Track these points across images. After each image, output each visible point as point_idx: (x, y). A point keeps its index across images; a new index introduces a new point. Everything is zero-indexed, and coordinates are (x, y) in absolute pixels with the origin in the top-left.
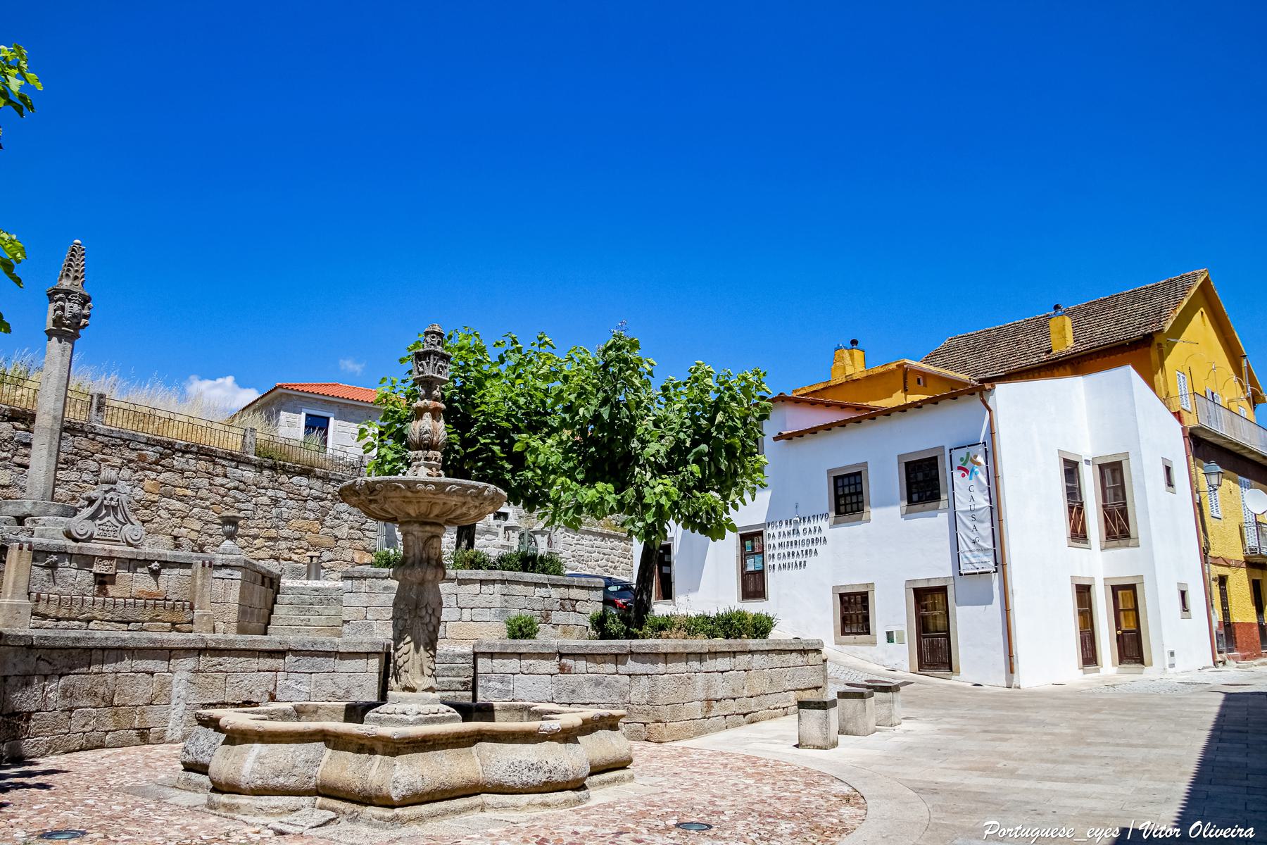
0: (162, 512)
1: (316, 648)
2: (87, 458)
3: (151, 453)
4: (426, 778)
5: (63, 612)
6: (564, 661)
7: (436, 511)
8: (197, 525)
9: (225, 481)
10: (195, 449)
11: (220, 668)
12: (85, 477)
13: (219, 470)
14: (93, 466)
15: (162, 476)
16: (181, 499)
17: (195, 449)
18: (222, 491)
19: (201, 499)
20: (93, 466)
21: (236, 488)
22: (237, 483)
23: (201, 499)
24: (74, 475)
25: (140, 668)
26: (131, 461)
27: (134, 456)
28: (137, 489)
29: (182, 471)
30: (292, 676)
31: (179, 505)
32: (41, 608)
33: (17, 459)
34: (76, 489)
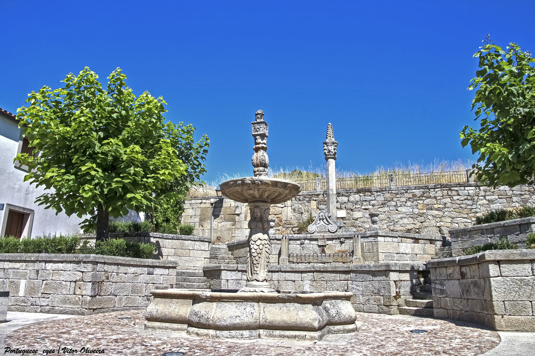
0: (429, 217)
1: (362, 269)
2: (390, 201)
3: (418, 192)
4: (159, 312)
5: (299, 260)
6: (463, 269)
7: (266, 194)
8: (449, 220)
9: (459, 197)
10: (439, 186)
11: (323, 279)
12: (391, 208)
13: (454, 193)
14: (394, 203)
15: (425, 202)
16: (438, 209)
17: (439, 186)
18: (458, 202)
19: (448, 208)
20: (394, 203)
21: (465, 199)
22: (466, 197)
23: (448, 208)
24: (386, 209)
25: (290, 278)
26: (409, 198)
27: (411, 196)
28: (415, 209)
29: (435, 197)
30: (354, 283)
31: (436, 212)
32: (291, 259)
33: (363, 207)
34: (389, 214)
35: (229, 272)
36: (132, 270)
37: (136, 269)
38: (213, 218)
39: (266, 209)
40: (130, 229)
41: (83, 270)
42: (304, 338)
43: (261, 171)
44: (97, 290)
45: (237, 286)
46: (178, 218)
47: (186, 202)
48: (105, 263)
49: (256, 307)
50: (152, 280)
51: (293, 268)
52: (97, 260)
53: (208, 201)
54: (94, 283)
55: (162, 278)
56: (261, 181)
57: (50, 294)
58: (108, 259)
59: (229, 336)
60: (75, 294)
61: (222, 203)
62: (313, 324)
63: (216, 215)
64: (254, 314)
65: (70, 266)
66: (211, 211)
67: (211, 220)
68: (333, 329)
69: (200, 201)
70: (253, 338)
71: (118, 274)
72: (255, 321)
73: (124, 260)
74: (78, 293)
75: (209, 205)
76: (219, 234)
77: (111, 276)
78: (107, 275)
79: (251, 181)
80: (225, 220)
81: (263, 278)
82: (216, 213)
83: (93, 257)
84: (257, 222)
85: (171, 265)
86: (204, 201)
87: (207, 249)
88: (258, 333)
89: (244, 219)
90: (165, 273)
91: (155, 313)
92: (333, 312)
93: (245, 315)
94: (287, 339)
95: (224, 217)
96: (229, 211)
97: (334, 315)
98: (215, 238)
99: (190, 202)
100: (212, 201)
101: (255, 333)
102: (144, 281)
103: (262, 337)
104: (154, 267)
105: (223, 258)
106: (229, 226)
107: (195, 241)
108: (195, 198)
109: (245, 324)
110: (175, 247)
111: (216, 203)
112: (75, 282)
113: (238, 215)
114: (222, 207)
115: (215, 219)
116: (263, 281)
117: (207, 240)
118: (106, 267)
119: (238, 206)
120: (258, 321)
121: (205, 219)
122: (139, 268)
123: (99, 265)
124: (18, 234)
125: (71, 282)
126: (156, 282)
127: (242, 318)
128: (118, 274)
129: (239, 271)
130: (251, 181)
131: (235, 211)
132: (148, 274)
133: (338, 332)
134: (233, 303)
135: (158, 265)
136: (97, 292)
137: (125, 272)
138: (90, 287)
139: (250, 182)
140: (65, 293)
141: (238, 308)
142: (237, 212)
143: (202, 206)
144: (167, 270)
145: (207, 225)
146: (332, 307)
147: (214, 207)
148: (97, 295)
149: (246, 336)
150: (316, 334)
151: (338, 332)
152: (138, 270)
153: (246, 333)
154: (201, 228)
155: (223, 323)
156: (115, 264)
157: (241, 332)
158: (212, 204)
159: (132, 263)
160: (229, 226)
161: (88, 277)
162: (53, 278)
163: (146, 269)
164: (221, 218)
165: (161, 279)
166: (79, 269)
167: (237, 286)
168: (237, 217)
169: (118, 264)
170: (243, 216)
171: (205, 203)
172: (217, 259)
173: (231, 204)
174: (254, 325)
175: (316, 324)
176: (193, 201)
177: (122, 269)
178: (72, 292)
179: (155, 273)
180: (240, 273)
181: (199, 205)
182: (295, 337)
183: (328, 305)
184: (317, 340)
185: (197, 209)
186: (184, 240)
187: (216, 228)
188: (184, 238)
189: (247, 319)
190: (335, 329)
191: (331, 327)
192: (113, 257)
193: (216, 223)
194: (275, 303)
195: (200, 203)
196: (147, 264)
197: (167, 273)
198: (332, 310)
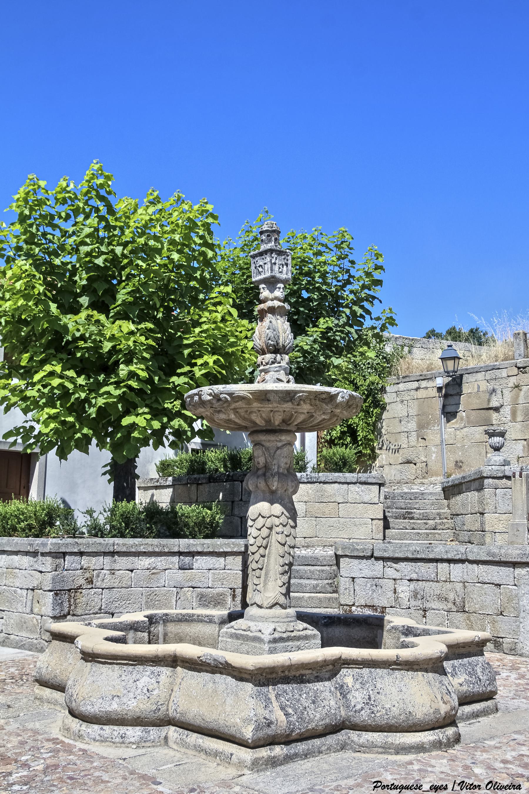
35: (356, 561)
36: (146, 562)
37: (153, 559)
38: (444, 420)
39: (278, 448)
40: (225, 467)
41: (40, 569)
42: (228, 759)
43: (267, 364)
44: (66, 604)
45: (374, 591)
46: (374, 425)
47: (388, 389)
48: (81, 554)
49: (163, 679)
50: (189, 580)
51: (494, 555)
52: (63, 550)
53: (430, 384)
54: (57, 593)
55: (210, 576)
56: (231, 394)
57: (4, 611)
58: (88, 545)
59: (98, 738)
60: (32, 612)
61: (460, 385)
62: (244, 730)
63: (449, 414)
64: (155, 692)
65: (26, 561)
66: (438, 403)
67: (440, 424)
68: (356, 739)
69: (415, 385)
70: (148, 744)
71: (112, 571)
72: (154, 707)
73: (124, 545)
74: (36, 610)
75: (434, 393)
76: (459, 455)
77: (98, 576)
78: (88, 575)
79: (210, 395)
80: (469, 422)
81: (272, 601)
82: (449, 409)
83: (51, 544)
84: (258, 477)
85: (229, 550)
86: (424, 384)
87: (376, 500)
88: (163, 735)
89: (509, 417)
90: (217, 566)
91: (44, 671)
92: (357, 698)
93: (131, 695)
94: (204, 757)
95: (467, 417)
96: (476, 403)
97: (358, 707)
98: (452, 465)
99: (395, 388)
100: (440, 381)
101: (154, 732)
102: (172, 584)
103: (171, 743)
104: (192, 554)
105: (426, 518)
106: (478, 436)
107: (348, 483)
108: (406, 379)
109: (130, 714)
110: (306, 499)
111: (447, 385)
112: (33, 590)
113: (497, 409)
114: (460, 394)
115: (448, 421)
116: (271, 607)
117: (374, 481)
118: (85, 561)
119: (494, 390)
120: (164, 708)
121: (428, 424)
122: (160, 559)
123: (67, 558)
124: (23, 491)
125: (27, 589)
126: (199, 585)
127: (125, 700)
128: (112, 571)
129: (377, 559)
130: (210, 395)
131: (489, 401)
132: (180, 568)
133: (369, 747)
134: (116, 667)
135: (200, 550)
136: (66, 610)
137: (130, 567)
138: (51, 601)
139: (209, 398)
140: (20, 610)
141: (123, 677)
142: (494, 403)
143: (421, 394)
144: (222, 560)
145: (433, 435)
146: (358, 686)
147: (446, 396)
148: (69, 614)
149: (132, 740)
150: (246, 755)
151: (369, 747)
152: (160, 562)
153: (134, 733)
154: (422, 443)
155: (89, 707)
156: (105, 554)
157: (122, 730)
158: (440, 389)
159: (142, 549)
160: (478, 436)
161: (47, 581)
162: (7, 582)
163: (175, 559)
164: (462, 419)
165: (210, 579)
166: (36, 567)
167: (374, 591)
168: (495, 416)
169: (112, 554)
170: (506, 411)
171: (426, 388)
172: (412, 518)
173: (479, 387)
174: (153, 716)
175: (248, 733)
176: (402, 386)
177: (123, 562)
178: (28, 610)
179: (195, 566)
180: (381, 562)
181: (413, 393)
182: (216, 754)
183: (349, 681)
184: (249, 769)
185: (411, 403)
186: (325, 483)
187: (451, 442)
188: (323, 479)
189: (133, 704)
190: (362, 741)
191: (354, 735)
192: (101, 540)
193: (450, 430)
194: (199, 671)
195: (417, 389)
196: (176, 549)
197: (222, 566)
198: (357, 694)
